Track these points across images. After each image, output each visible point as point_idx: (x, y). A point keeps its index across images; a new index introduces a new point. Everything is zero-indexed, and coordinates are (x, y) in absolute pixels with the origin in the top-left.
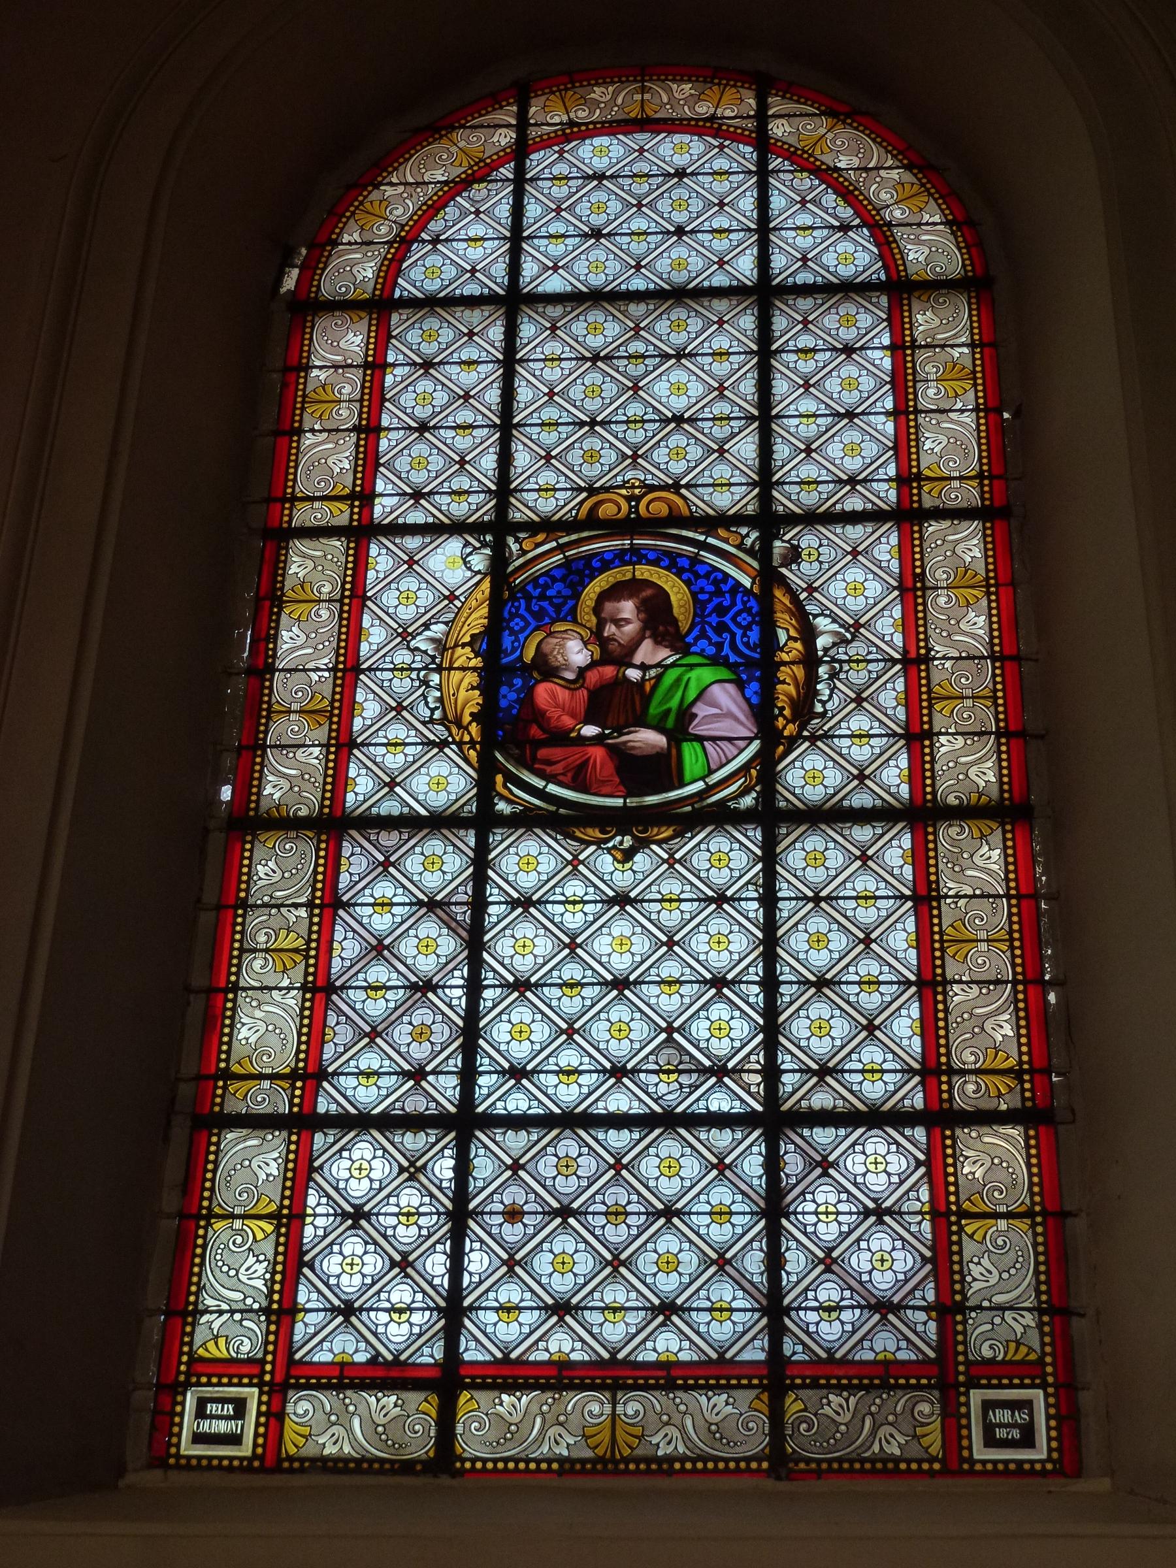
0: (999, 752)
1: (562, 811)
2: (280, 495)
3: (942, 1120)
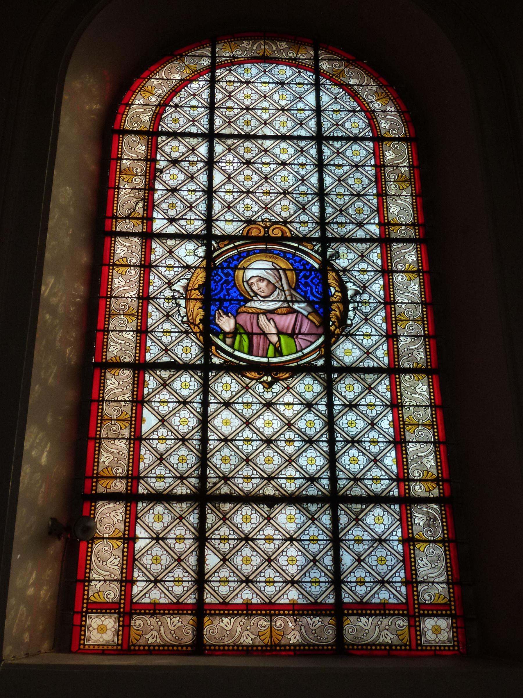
0: (426, 345)
1: (241, 363)
2: (108, 263)
3: (407, 502)
